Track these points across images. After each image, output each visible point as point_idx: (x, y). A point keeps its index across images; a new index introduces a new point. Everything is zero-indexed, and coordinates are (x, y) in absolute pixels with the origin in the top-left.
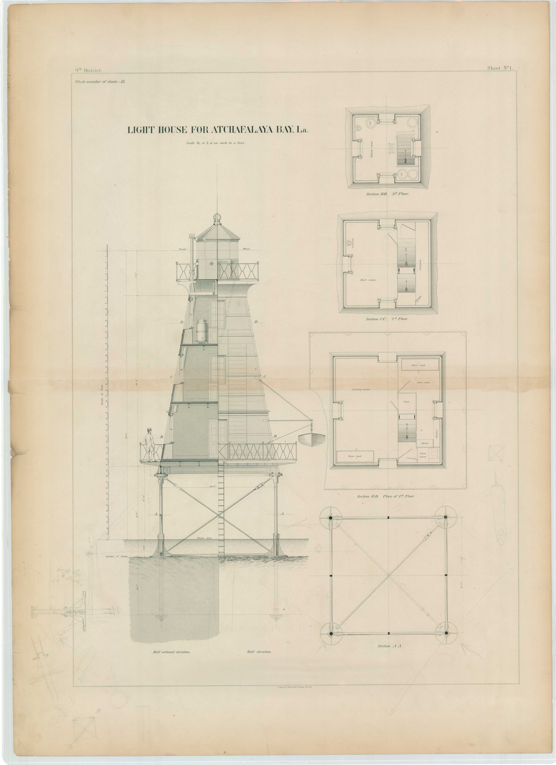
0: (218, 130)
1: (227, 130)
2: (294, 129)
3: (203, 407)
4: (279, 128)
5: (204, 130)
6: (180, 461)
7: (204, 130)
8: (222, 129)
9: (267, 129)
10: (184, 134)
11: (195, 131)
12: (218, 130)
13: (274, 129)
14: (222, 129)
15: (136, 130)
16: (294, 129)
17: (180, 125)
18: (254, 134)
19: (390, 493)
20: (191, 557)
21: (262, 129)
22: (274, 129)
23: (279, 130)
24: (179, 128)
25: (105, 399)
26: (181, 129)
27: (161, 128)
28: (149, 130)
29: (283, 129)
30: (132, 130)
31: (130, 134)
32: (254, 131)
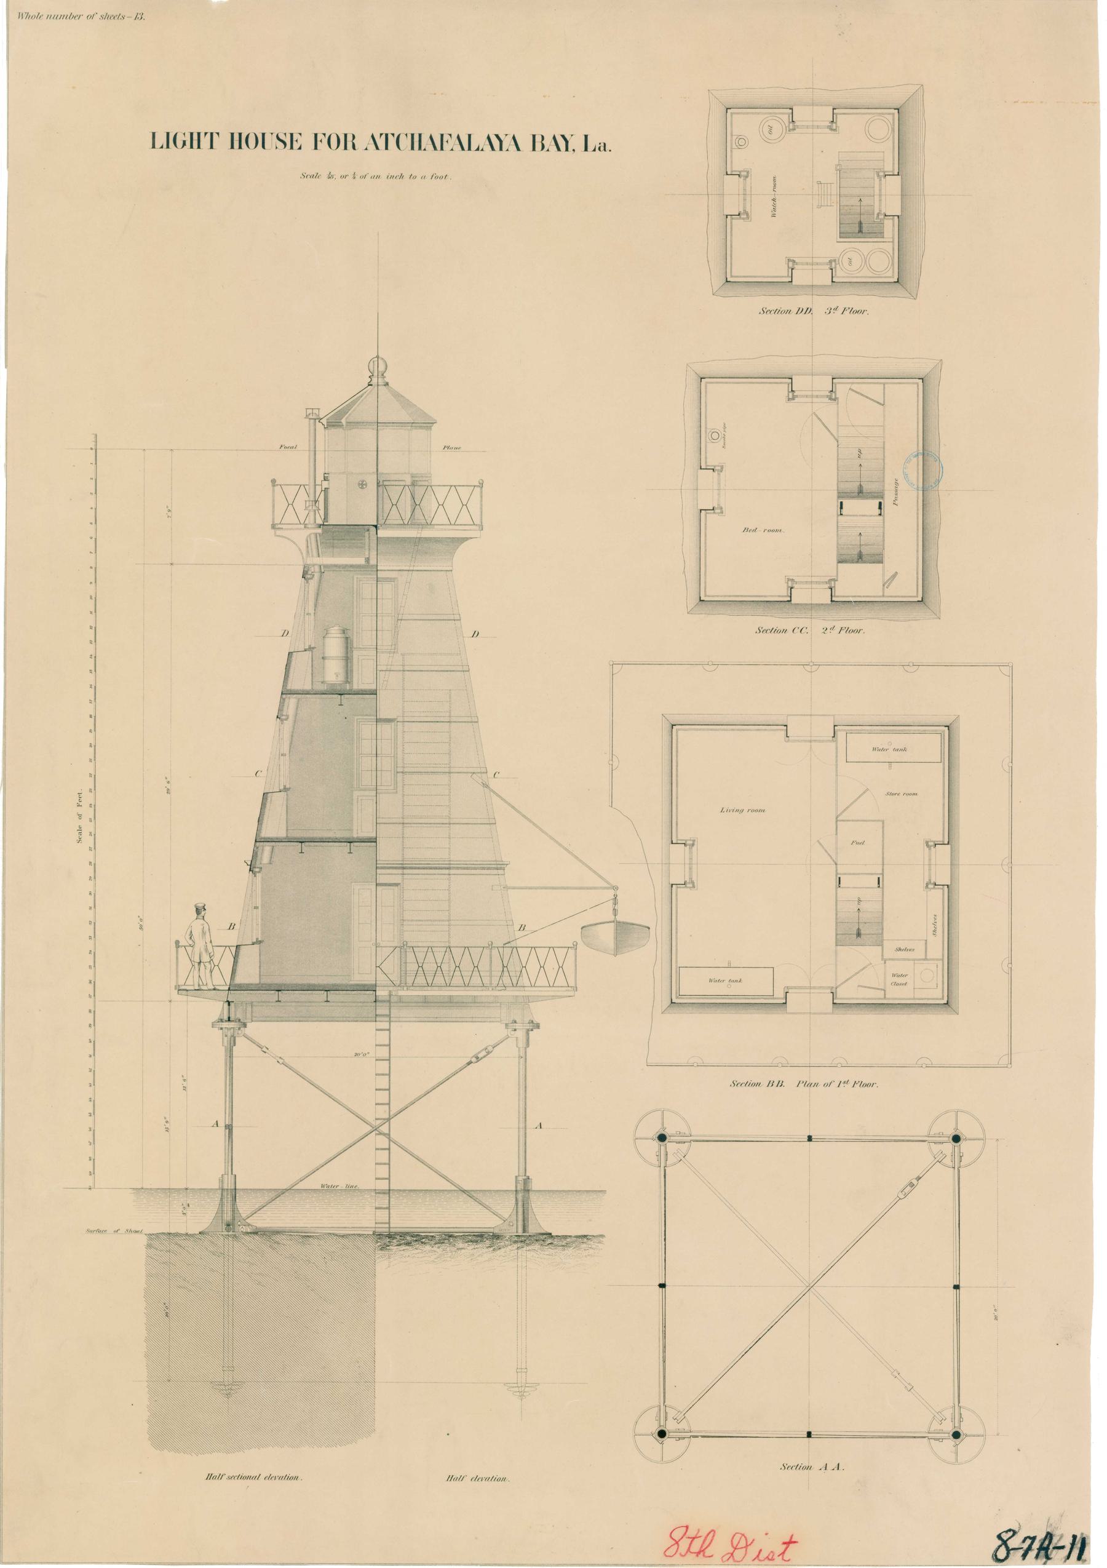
0: (381, 142)
2: (577, 143)
4: (538, 139)
8: (392, 141)
9: (508, 142)
10: (295, 151)
11: (323, 145)
12: (381, 142)
13: (525, 143)
14: (392, 141)
16: (577, 143)
18: (472, 153)
21: (495, 142)
22: (525, 143)
23: (538, 146)
24: (282, 137)
26: (288, 140)
27: (236, 137)
29: (549, 141)
30: (161, 140)
31: (157, 151)
32: (474, 147)
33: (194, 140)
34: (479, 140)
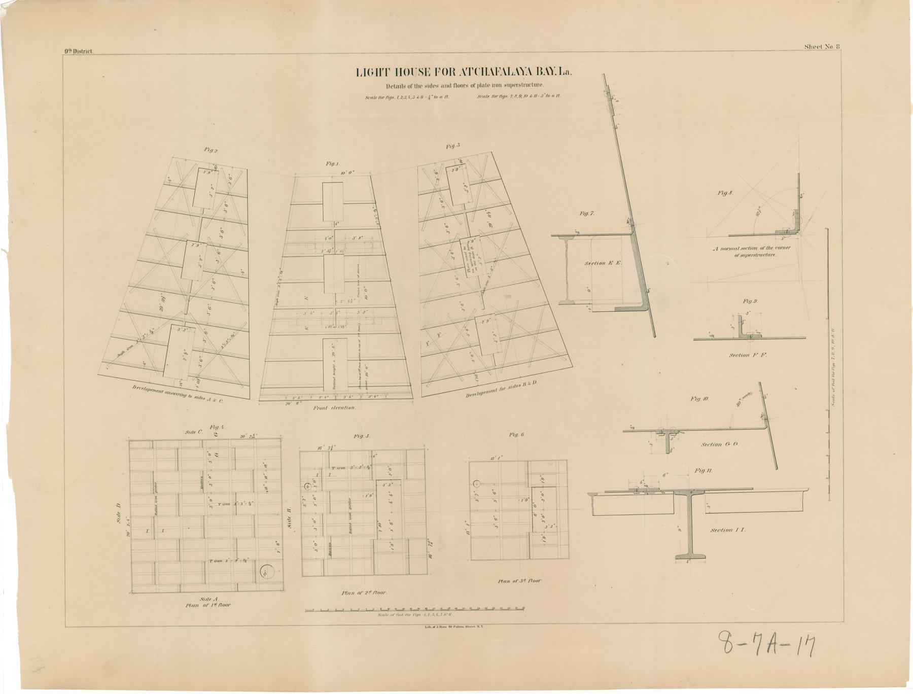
1: (479, 72)
2: (556, 71)
3: (797, 186)
5: (450, 72)
6: (713, 338)
7: (450, 72)
8: (473, 72)
12: (467, 72)
13: (534, 71)
14: (473, 72)
15: (367, 72)
16: (556, 71)
17: (422, 66)
19: (831, 373)
20: (749, 248)
25: (210, 603)
28: (383, 72)
29: (544, 71)
30: (361, 72)
33: (378, 72)
34: (513, 70)
